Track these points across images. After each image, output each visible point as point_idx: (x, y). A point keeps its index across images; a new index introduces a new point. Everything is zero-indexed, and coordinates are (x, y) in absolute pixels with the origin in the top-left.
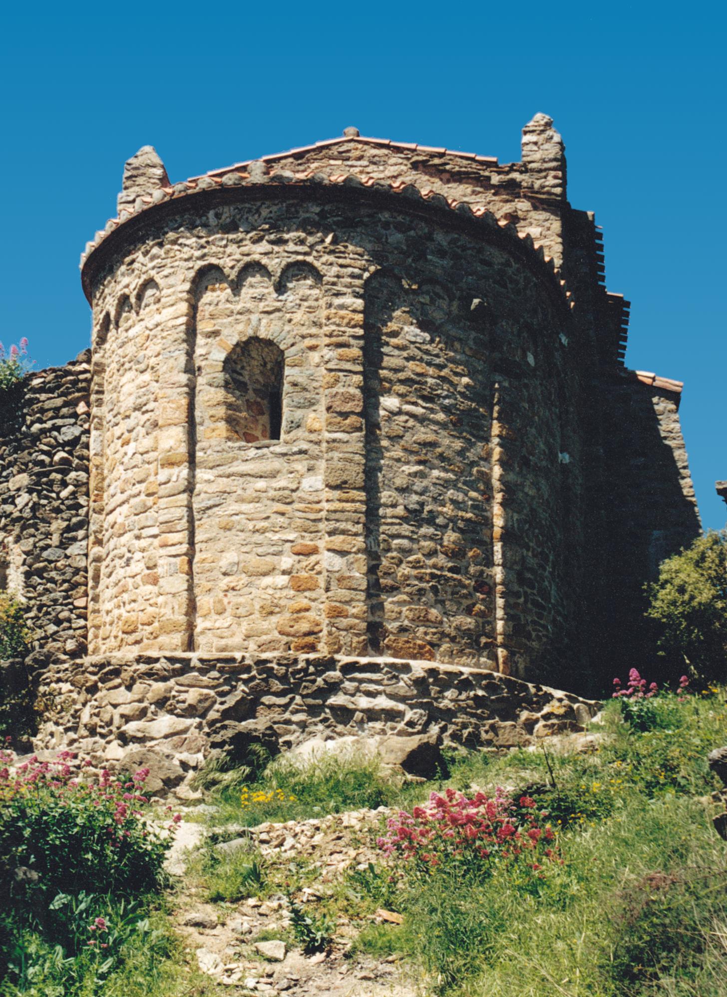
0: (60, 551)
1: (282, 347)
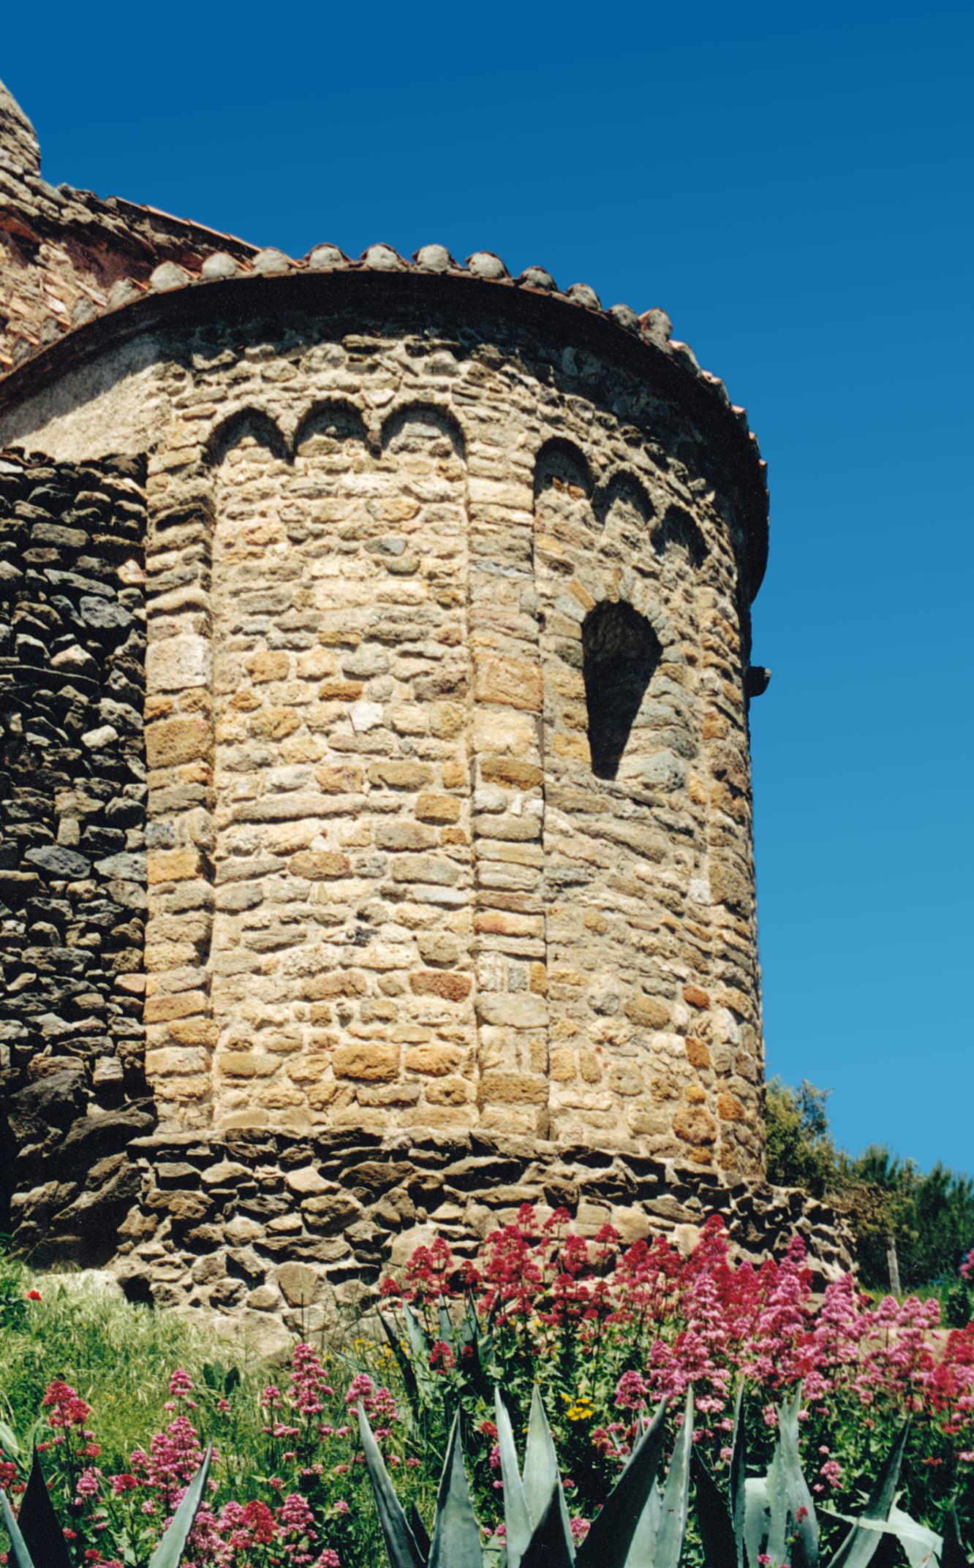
0: (79, 861)
1: (662, 639)
